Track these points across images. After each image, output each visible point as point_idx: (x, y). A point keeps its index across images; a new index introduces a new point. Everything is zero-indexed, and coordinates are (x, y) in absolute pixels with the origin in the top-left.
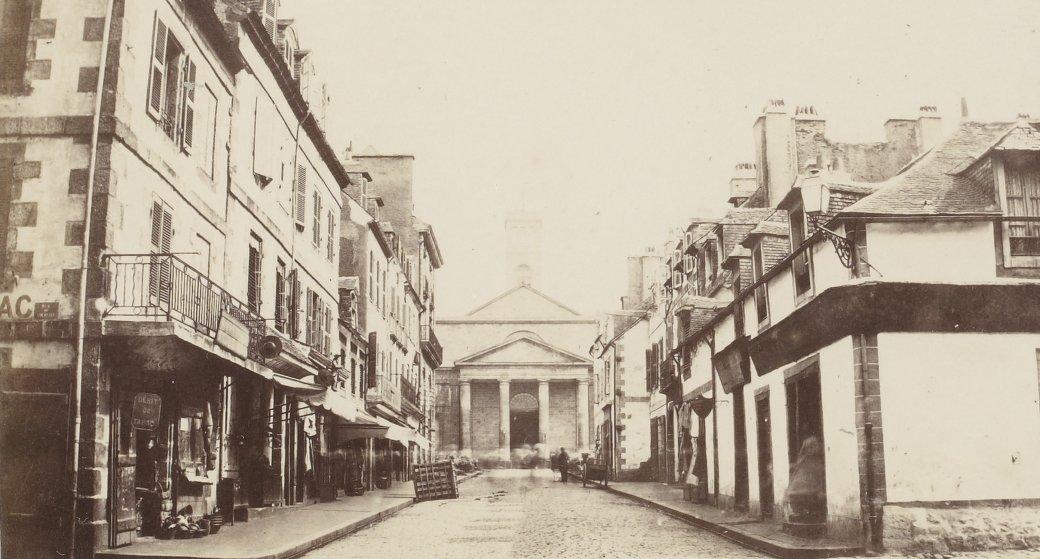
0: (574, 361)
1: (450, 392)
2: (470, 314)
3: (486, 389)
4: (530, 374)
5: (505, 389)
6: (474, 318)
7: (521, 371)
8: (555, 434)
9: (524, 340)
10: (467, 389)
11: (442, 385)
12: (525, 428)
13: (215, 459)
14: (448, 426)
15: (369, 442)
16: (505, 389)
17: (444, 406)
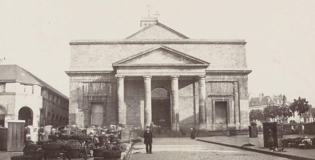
0: (196, 63)
1: (111, 87)
2: (128, 38)
3: (135, 84)
4: (165, 72)
5: (148, 83)
6: (131, 40)
7: (159, 71)
8: (183, 108)
9: (161, 49)
10: (121, 83)
11: (105, 82)
12: (163, 108)
13: (214, 115)
14: (109, 109)
15: (231, 103)
16: (148, 83)
17: (107, 97)
